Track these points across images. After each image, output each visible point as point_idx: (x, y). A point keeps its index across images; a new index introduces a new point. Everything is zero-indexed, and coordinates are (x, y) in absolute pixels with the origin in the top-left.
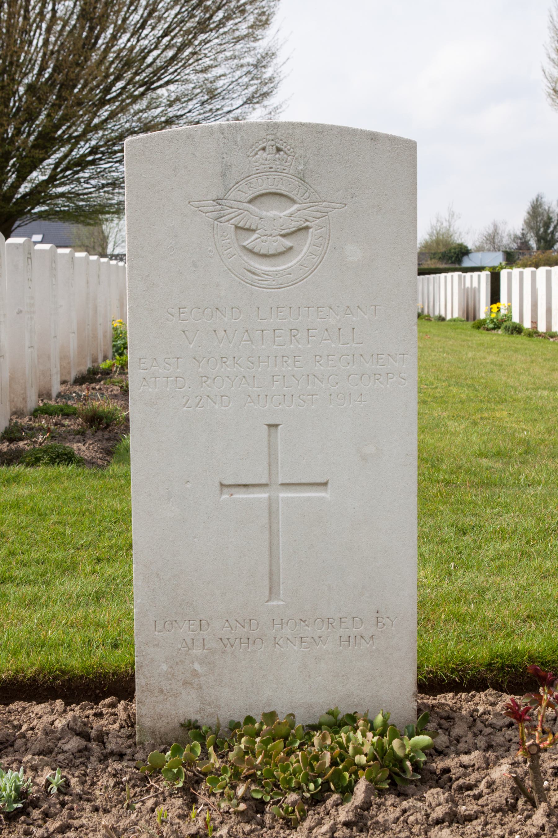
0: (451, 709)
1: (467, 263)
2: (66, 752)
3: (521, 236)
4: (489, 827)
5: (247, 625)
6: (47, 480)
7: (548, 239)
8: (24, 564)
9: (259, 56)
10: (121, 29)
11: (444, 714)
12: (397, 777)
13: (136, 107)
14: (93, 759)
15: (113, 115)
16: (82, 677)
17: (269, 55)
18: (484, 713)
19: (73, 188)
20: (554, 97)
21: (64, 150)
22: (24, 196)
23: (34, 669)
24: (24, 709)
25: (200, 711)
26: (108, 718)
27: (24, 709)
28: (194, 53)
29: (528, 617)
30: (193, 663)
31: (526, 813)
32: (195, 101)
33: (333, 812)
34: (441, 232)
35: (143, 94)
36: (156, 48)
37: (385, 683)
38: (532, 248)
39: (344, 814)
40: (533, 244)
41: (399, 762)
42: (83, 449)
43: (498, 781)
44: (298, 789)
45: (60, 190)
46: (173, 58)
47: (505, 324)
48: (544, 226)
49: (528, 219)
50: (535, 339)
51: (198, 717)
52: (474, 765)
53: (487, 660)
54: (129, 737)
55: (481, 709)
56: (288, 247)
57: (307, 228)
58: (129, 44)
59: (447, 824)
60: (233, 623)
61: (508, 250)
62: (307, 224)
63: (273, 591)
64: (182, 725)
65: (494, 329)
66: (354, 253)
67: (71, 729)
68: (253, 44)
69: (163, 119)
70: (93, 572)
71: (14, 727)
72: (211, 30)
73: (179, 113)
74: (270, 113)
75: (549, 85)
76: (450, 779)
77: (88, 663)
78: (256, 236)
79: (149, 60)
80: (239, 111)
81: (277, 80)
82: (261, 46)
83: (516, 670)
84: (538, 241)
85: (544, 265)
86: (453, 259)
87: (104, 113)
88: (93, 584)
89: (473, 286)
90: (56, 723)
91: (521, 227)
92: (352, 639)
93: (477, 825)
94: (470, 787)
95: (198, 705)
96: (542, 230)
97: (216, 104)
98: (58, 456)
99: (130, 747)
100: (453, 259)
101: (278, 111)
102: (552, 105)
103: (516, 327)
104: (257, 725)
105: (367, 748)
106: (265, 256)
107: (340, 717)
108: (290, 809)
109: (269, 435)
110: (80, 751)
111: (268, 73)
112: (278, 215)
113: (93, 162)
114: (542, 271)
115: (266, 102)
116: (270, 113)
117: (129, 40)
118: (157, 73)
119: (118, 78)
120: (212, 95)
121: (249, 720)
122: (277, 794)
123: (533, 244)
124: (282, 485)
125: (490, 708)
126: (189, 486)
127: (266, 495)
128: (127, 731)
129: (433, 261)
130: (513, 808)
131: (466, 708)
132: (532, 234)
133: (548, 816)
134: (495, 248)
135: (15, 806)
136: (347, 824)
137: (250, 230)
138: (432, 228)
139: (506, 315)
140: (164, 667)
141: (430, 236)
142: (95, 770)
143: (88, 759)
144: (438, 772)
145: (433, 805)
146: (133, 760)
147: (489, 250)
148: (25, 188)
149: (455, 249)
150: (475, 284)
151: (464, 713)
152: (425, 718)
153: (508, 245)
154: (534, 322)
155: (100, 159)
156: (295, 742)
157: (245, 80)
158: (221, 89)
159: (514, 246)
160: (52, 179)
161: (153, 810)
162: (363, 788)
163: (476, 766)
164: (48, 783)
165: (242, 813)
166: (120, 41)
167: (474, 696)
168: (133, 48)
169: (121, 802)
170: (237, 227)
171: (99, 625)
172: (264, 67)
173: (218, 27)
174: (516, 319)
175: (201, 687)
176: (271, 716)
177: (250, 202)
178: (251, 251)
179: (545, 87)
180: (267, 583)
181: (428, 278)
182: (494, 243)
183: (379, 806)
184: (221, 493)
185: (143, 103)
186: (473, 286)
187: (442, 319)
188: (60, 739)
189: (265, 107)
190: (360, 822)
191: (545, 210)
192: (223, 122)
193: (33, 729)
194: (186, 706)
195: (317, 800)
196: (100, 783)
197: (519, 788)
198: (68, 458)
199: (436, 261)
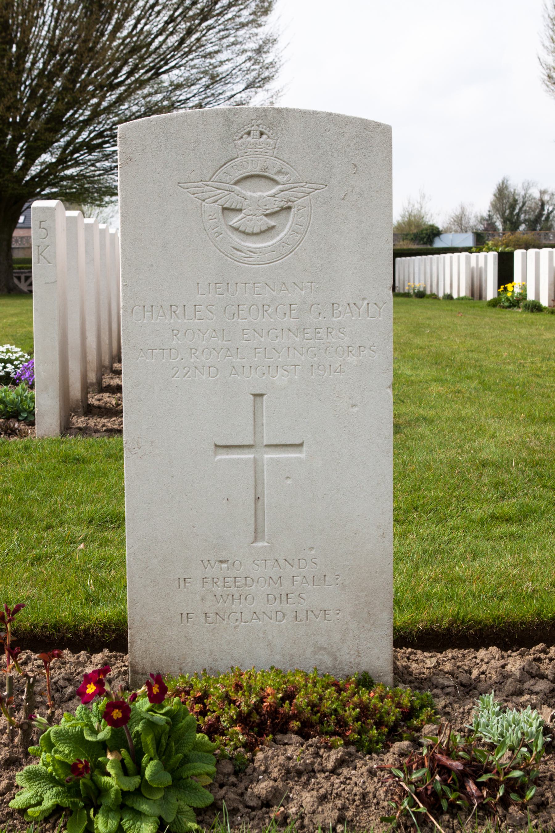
1: (438, 244)
3: (487, 218)
9: (261, 42)
16: (492, 626)
17: (269, 41)
20: (548, 83)
21: (73, 133)
22: (33, 178)
23: (447, 620)
24: (464, 656)
27: (464, 656)
28: (198, 40)
34: (413, 214)
36: (161, 34)
38: (499, 229)
40: (499, 225)
45: (68, 172)
48: (509, 208)
56: (270, 226)
57: (289, 208)
62: (289, 204)
65: (509, 307)
67: (528, 672)
68: (255, 30)
74: (272, 97)
75: (544, 72)
78: (242, 215)
81: (277, 66)
82: (262, 32)
85: (534, 247)
86: (425, 240)
87: (111, 97)
89: (480, 266)
91: (488, 209)
96: (508, 212)
97: (218, 88)
100: (425, 240)
101: (279, 95)
102: (546, 91)
103: (535, 306)
109: (254, 401)
111: (268, 58)
112: (262, 194)
115: (267, 86)
116: (272, 97)
120: (214, 79)
123: (499, 225)
124: (267, 446)
127: (252, 456)
129: (406, 241)
132: (498, 216)
134: (464, 230)
138: (404, 209)
139: (520, 294)
141: (403, 217)
147: (456, 232)
148: (34, 170)
149: (427, 230)
150: (482, 264)
153: (475, 226)
155: (108, 142)
158: (226, 74)
160: (62, 162)
173: (220, 14)
174: (531, 297)
179: (540, 73)
181: (431, 258)
182: (461, 224)
186: (480, 266)
187: (449, 297)
192: (224, 106)
193: (483, 673)
199: (409, 242)
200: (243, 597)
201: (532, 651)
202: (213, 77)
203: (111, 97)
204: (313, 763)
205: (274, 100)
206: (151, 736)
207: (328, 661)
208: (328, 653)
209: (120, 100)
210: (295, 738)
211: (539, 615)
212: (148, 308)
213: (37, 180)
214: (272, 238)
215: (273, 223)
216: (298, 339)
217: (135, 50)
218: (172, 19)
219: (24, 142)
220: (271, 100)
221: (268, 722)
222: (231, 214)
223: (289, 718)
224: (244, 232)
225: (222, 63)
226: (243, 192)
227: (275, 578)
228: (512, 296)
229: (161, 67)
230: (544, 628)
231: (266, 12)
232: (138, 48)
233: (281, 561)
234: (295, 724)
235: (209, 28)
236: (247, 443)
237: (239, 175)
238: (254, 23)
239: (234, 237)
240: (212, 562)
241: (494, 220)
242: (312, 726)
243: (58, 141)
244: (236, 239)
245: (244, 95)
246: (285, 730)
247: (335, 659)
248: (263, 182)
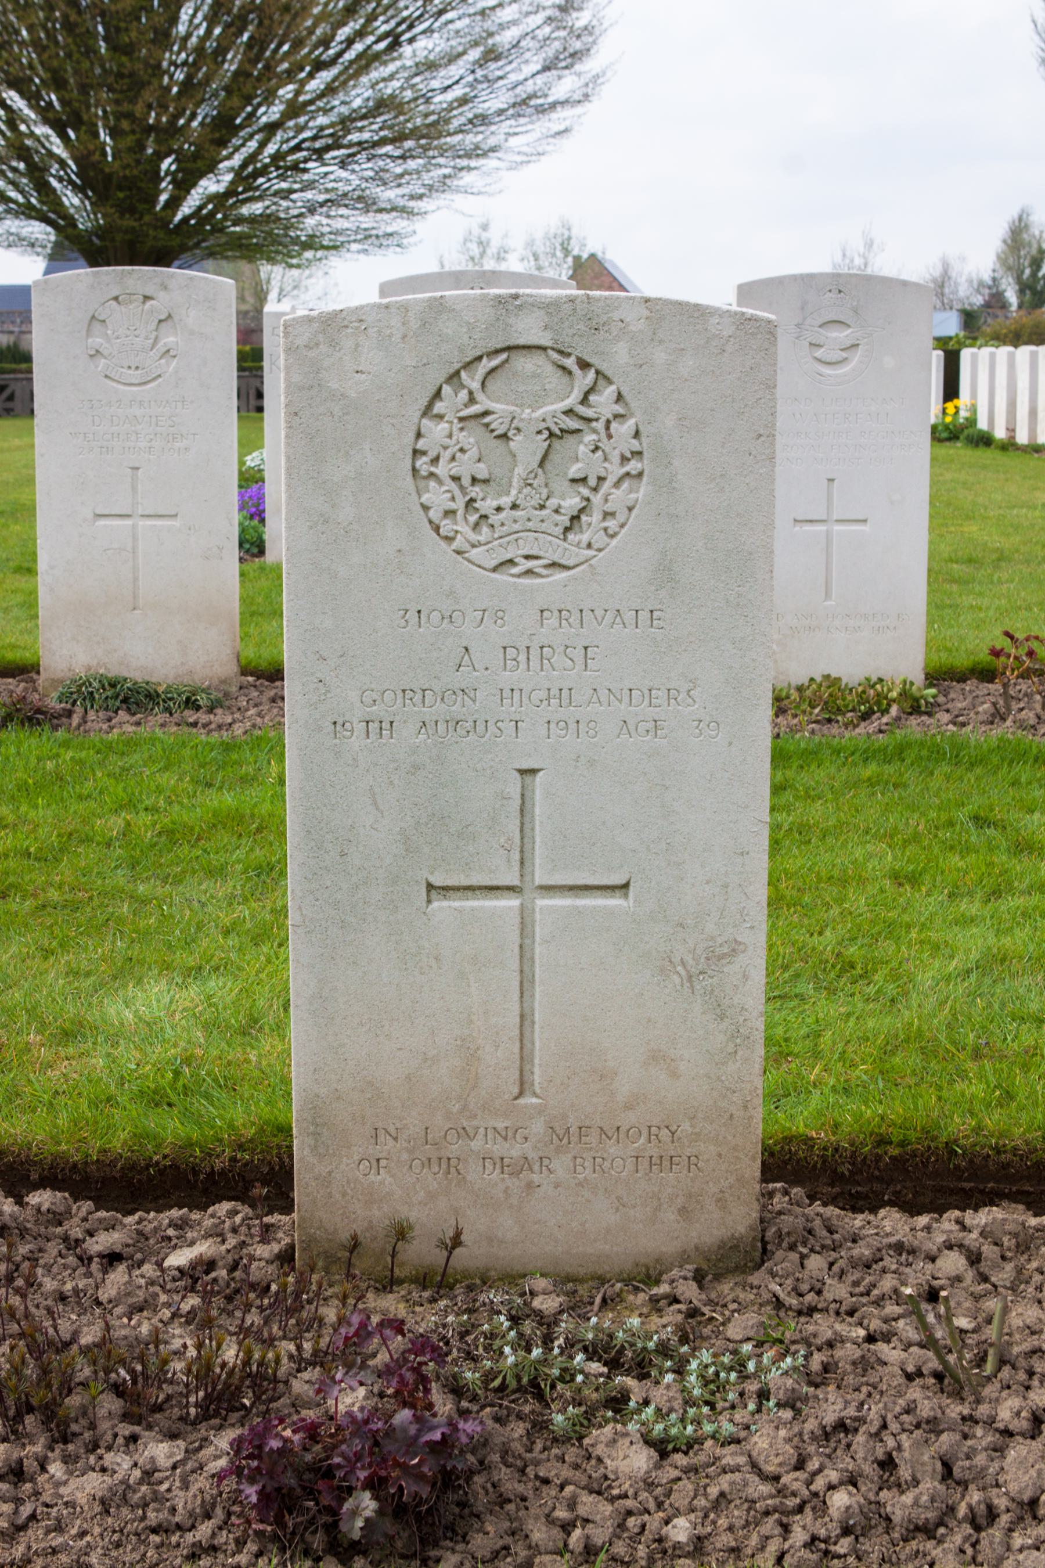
3: (990, 283)
7: (1039, 288)
19: (268, 207)
38: (1010, 305)
40: (1012, 297)
44: (853, 710)
47: (966, 432)
48: (1031, 266)
49: (1003, 252)
50: (1011, 454)
61: (968, 307)
63: (828, 595)
65: (949, 439)
74: (587, 85)
81: (597, 32)
84: (1021, 292)
106: (829, 363)
114: (1024, 352)
115: (578, 67)
116: (587, 85)
120: (492, 55)
123: (1012, 297)
130: (992, 723)
132: (1010, 280)
139: (967, 419)
154: (1011, 430)
159: (978, 300)
174: (982, 425)
177: (820, 326)
178: (819, 360)
182: (943, 295)
189: (579, 75)
191: (1034, 236)
203: (316, 84)
205: (589, 91)
213: (193, 222)
219: (173, 157)
220: (585, 90)
228: (953, 422)
241: (1003, 287)
243: (229, 157)
245: (540, 80)
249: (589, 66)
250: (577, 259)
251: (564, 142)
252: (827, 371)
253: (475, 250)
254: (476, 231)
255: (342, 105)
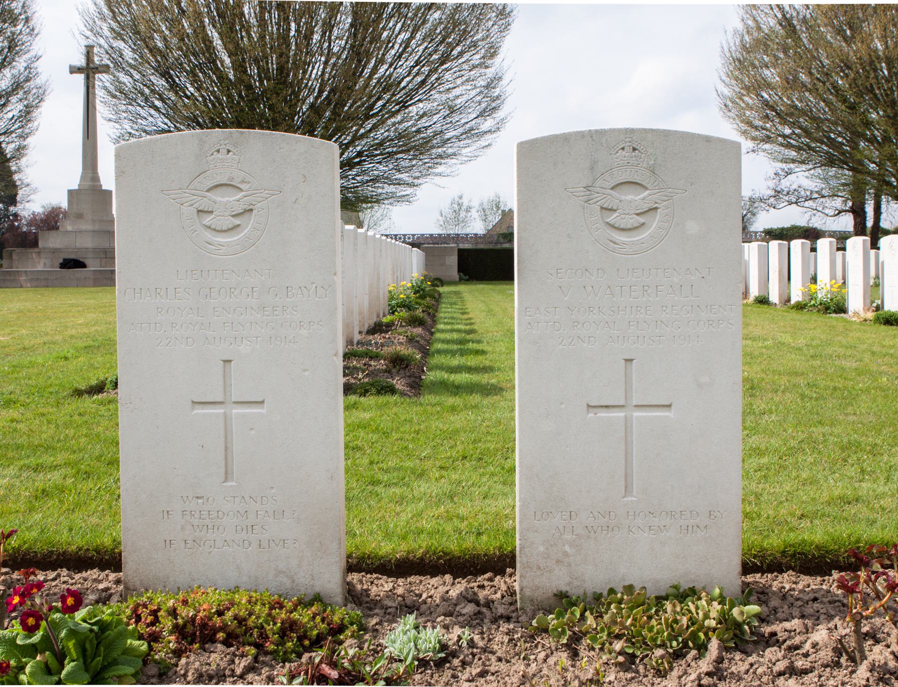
0: (764, 585)
2: (464, 615)
4: (823, 679)
5: (607, 516)
6: (380, 407)
8: (387, 471)
10: (381, 61)
11: (761, 590)
12: (740, 639)
13: (393, 120)
14: (486, 621)
15: (374, 128)
16: (459, 558)
18: (790, 590)
23: (421, 551)
24: (421, 582)
25: (569, 584)
26: (491, 589)
27: (421, 582)
28: (437, 79)
29: (802, 515)
30: (564, 545)
31: (850, 669)
32: (438, 116)
33: (693, 664)
35: (398, 111)
36: (408, 75)
37: (717, 563)
39: (705, 665)
41: (738, 625)
42: (399, 383)
43: (820, 643)
44: (663, 645)
46: (423, 82)
51: (568, 588)
52: (795, 630)
53: (782, 549)
54: (511, 604)
55: (787, 587)
57: (251, 210)
58: (388, 73)
59: (787, 675)
60: (596, 514)
62: (251, 207)
64: (555, 595)
66: (692, 227)
67: (464, 597)
68: (483, 70)
69: (414, 129)
70: (442, 477)
71: (416, 595)
72: (452, 60)
73: (427, 125)
76: (778, 641)
77: (464, 546)
78: (616, 214)
79: (403, 84)
80: (474, 122)
83: (806, 556)
88: (445, 486)
90: (450, 593)
92: (690, 528)
93: (812, 677)
94: (797, 647)
95: (567, 579)
98: (382, 389)
99: (513, 612)
104: (619, 595)
105: (714, 614)
106: (623, 230)
107: (681, 590)
108: (660, 661)
109: (626, 368)
110: (475, 614)
111: (497, 92)
112: (635, 198)
113: (359, 163)
115: (494, 115)
117: (387, 70)
118: (410, 95)
119: (379, 99)
120: (452, 110)
121: (612, 591)
122: (645, 649)
124: (636, 406)
125: (794, 586)
126: (563, 406)
128: (507, 599)
130: (838, 665)
131: (775, 586)
133: (871, 671)
135: (440, 655)
136: (709, 674)
137: (612, 210)
140: (542, 549)
142: (490, 629)
143: (482, 620)
144: (766, 635)
145: (773, 661)
146: (518, 622)
151: (774, 589)
152: (748, 594)
155: (365, 161)
156: (651, 609)
157: (478, 98)
161: (545, 660)
162: (716, 646)
163: (798, 631)
164: (460, 638)
165: (617, 664)
166: (381, 70)
167: (777, 577)
168: (390, 76)
169: (518, 654)
170: (602, 208)
171: (462, 519)
172: (494, 88)
175: (570, 565)
176: (629, 589)
177: (612, 189)
178: (613, 226)
180: (623, 483)
183: (730, 660)
184: (588, 412)
185: (399, 117)
188: (456, 605)
190: (717, 673)
193: (431, 597)
194: (558, 580)
195: (678, 655)
196: (497, 639)
197: (839, 650)
198: (392, 390)
200: (216, 528)
201: (479, 579)
202: (450, 107)
204: (225, 669)
206: (74, 641)
207: (288, 583)
208: (287, 576)
209: (374, 128)
210: (220, 647)
211: (500, 548)
212: (137, 290)
214: (238, 234)
215: (643, 221)
216: (259, 316)
217: (386, 90)
218: (417, 63)
221: (197, 634)
222: (205, 215)
223: (215, 631)
224: (214, 230)
225: (457, 97)
226: (214, 197)
227: (242, 512)
229: (407, 102)
230: (504, 560)
231: (493, 55)
232: (389, 85)
233: (247, 498)
234: (221, 635)
235: (447, 70)
236: (218, 400)
237: (210, 184)
238: (483, 65)
239: (206, 233)
240: (190, 498)
242: (237, 637)
244: (209, 235)
246: (213, 641)
247: (293, 581)
248: (230, 189)
249: (500, 114)
250: (503, 211)
251: (488, 151)
252: (621, 238)
253: (456, 207)
254: (457, 199)
255: (381, 134)
